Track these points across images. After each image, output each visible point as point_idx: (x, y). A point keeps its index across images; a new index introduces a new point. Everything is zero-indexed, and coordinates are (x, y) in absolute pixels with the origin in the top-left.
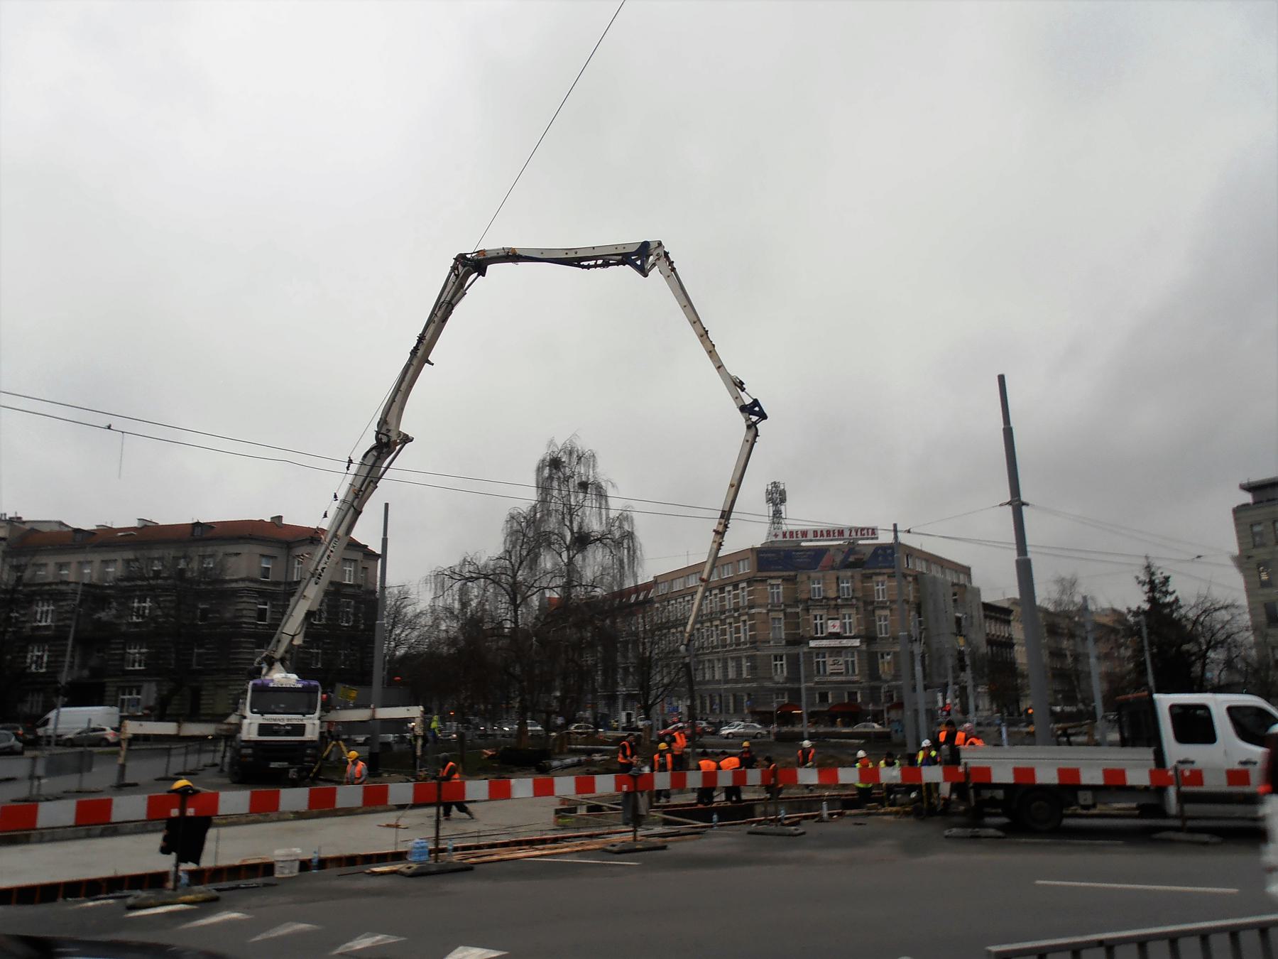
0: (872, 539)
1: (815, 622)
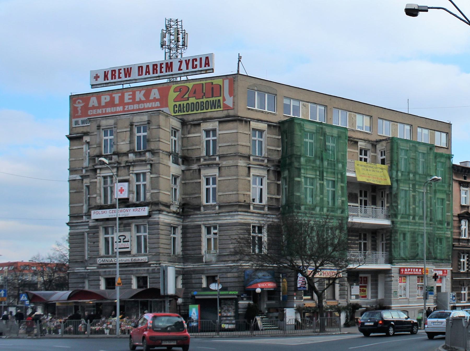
0: (206, 71)
1: (214, 186)
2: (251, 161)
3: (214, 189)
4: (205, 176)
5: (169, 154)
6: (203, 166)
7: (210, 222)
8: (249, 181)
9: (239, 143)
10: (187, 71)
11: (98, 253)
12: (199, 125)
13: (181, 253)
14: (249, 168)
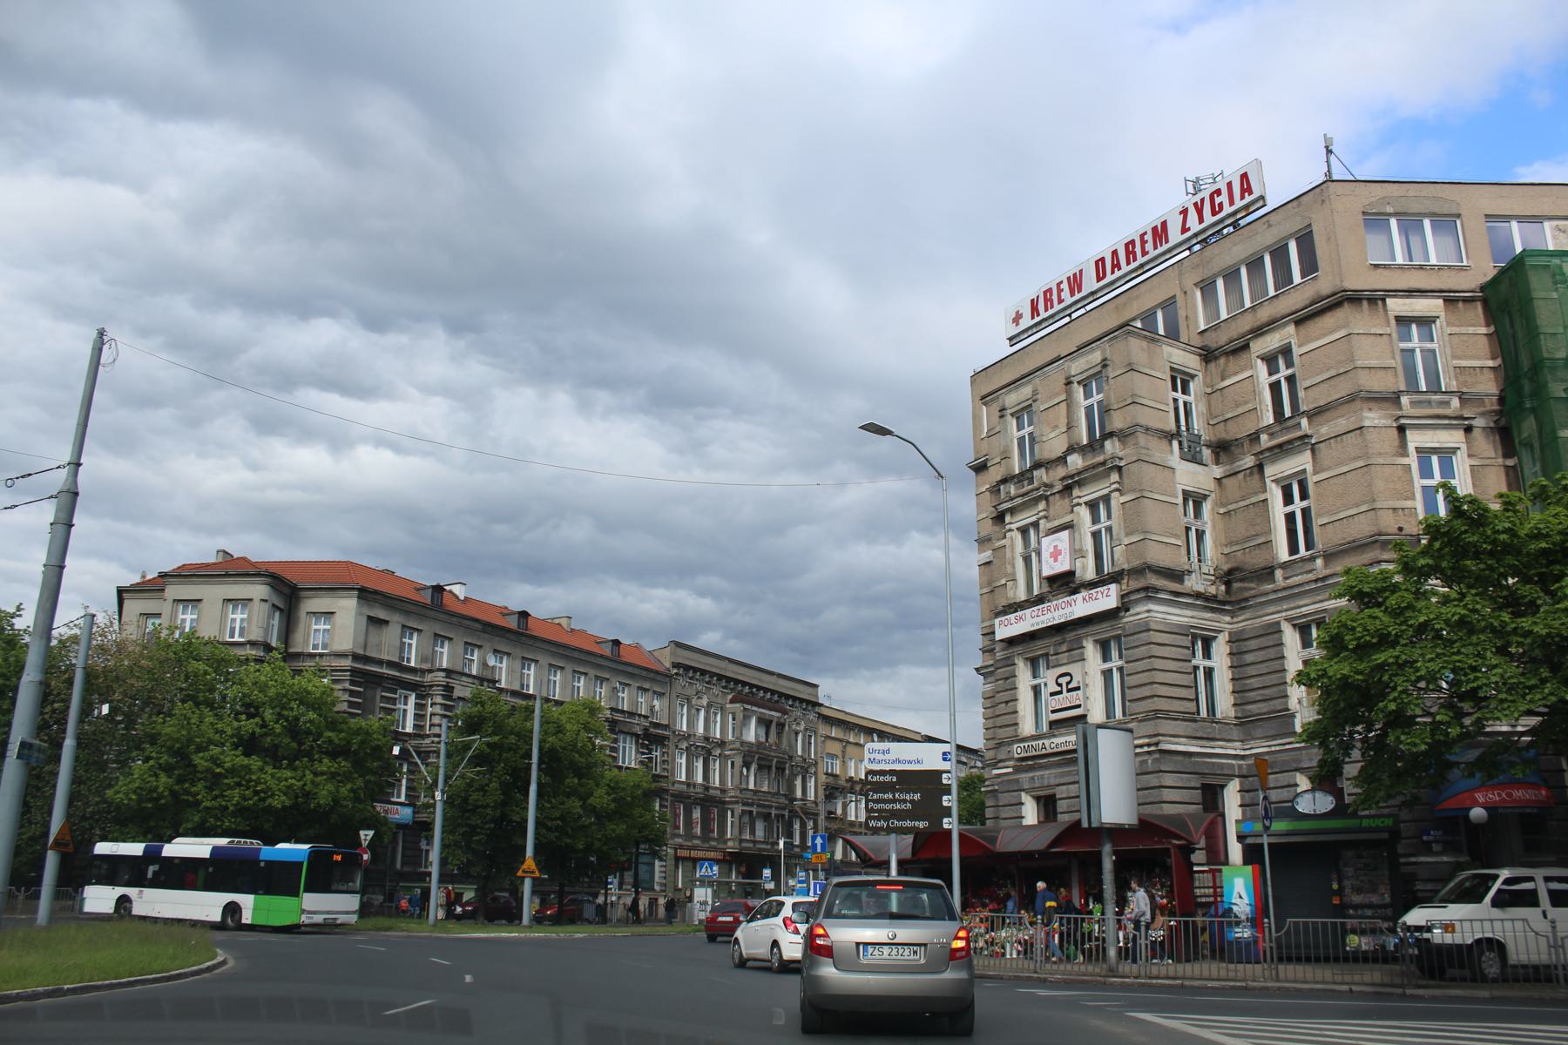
2: (1404, 408)
3: (1306, 512)
4: (1276, 481)
5: (1170, 436)
7: (1303, 609)
8: (1408, 468)
9: (1359, 363)
11: (1016, 730)
12: (1246, 347)
13: (1232, 713)
14: (1402, 429)
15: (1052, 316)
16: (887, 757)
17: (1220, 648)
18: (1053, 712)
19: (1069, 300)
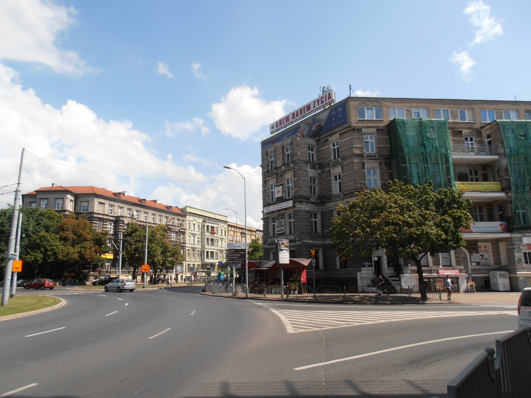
5: (307, 162)
6: (331, 167)
8: (364, 173)
9: (354, 146)
10: (319, 106)
15: (282, 127)
16: (232, 246)
17: (319, 216)
18: (277, 231)
19: (286, 123)
